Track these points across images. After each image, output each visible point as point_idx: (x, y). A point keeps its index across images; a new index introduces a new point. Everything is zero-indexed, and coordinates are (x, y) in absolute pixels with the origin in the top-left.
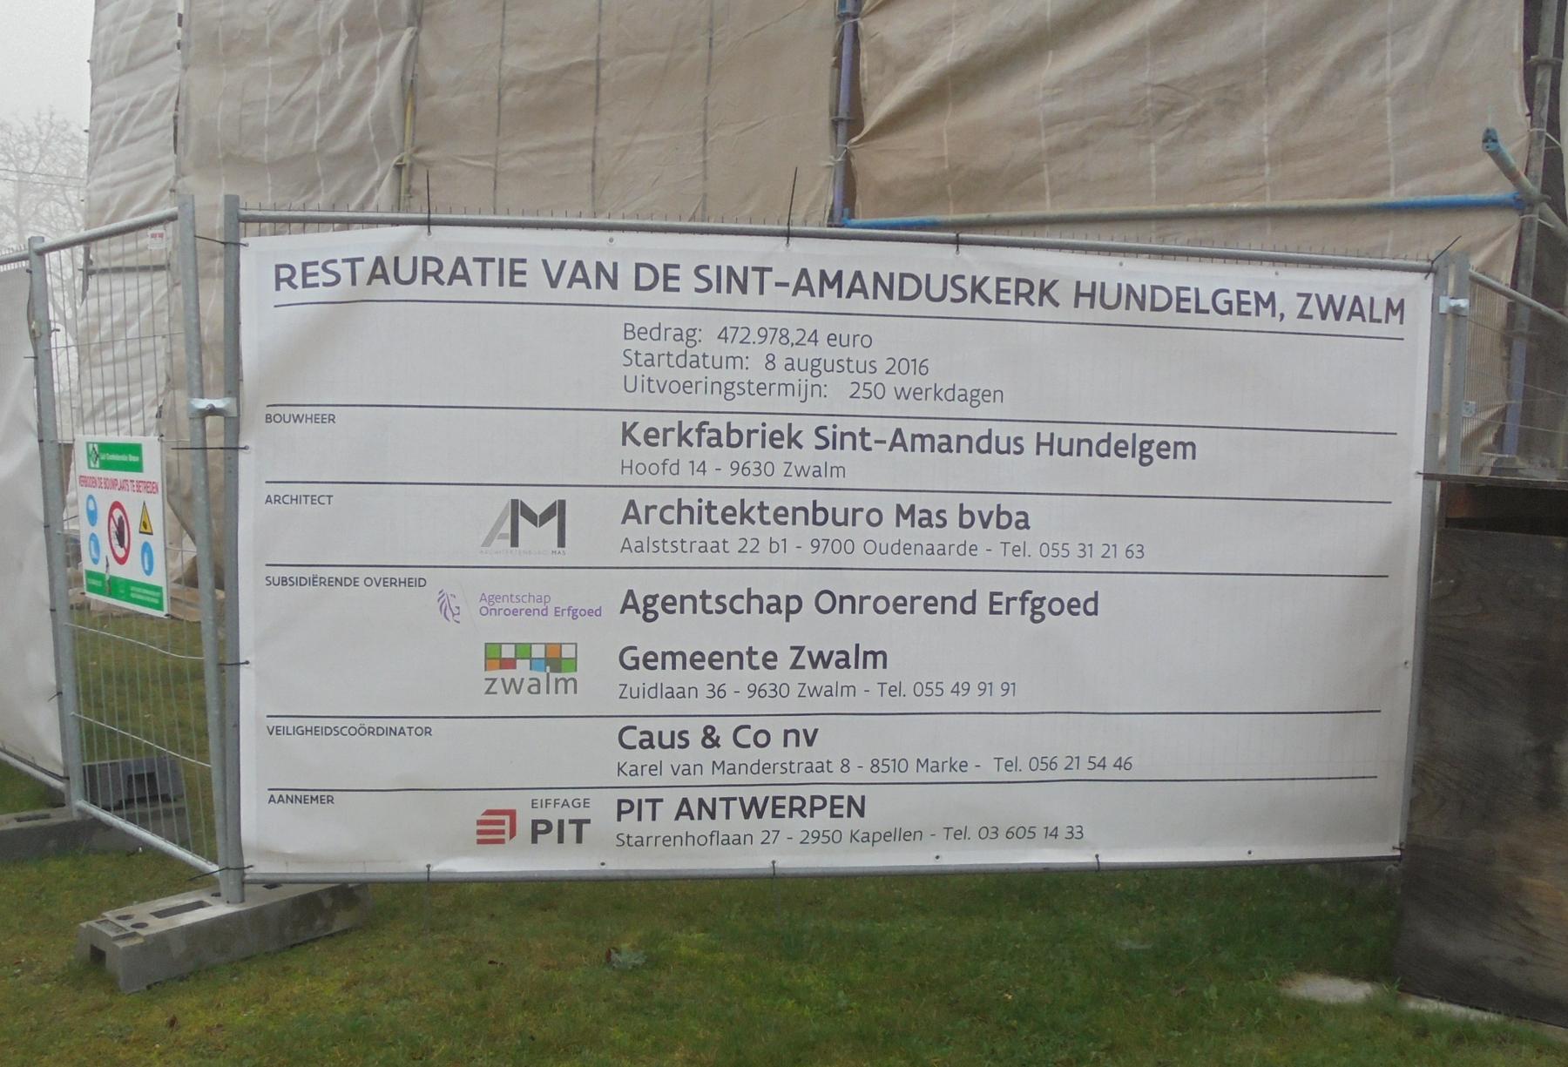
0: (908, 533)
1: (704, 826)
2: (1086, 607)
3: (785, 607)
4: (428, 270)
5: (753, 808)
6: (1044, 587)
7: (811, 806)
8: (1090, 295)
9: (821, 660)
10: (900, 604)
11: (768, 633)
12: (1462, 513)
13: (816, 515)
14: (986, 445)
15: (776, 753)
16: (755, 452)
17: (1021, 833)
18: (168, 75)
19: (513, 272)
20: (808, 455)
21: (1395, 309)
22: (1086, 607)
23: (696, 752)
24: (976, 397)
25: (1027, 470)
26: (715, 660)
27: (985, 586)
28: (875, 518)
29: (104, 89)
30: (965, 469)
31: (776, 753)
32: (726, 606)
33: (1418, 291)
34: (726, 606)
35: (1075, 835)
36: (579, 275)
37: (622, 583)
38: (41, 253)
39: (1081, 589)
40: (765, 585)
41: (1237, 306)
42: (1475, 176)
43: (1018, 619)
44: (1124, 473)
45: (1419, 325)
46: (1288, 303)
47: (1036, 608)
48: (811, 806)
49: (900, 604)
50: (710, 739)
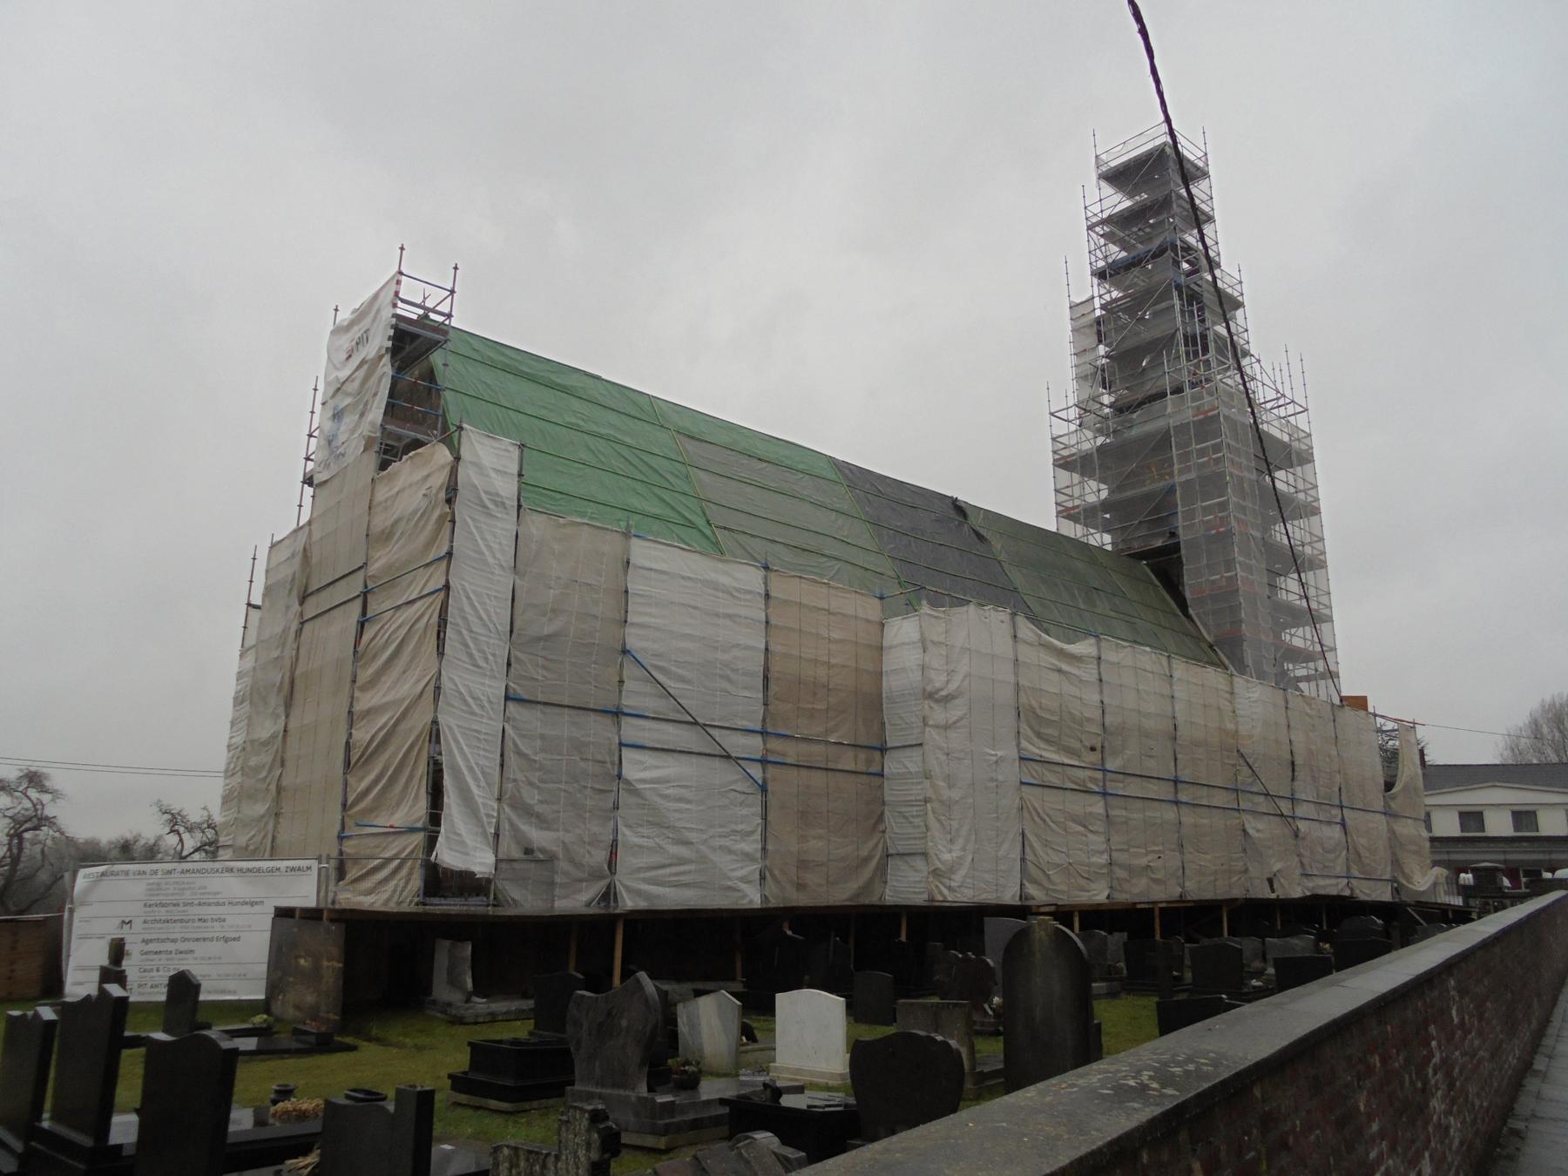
2: (238, 939)
3: (174, 941)
8: (240, 870)
12: (1116, 253)
13: (181, 921)
14: (218, 904)
15: (148, 990)
17: (223, 992)
18: (238, 778)
19: (127, 873)
20: (181, 908)
21: (309, 868)
22: (238, 939)
30: (212, 910)
31: (148, 990)
32: (163, 941)
33: (314, 864)
35: (235, 993)
37: (141, 937)
38: (767, 596)
43: (222, 943)
44: (247, 909)
47: (226, 940)
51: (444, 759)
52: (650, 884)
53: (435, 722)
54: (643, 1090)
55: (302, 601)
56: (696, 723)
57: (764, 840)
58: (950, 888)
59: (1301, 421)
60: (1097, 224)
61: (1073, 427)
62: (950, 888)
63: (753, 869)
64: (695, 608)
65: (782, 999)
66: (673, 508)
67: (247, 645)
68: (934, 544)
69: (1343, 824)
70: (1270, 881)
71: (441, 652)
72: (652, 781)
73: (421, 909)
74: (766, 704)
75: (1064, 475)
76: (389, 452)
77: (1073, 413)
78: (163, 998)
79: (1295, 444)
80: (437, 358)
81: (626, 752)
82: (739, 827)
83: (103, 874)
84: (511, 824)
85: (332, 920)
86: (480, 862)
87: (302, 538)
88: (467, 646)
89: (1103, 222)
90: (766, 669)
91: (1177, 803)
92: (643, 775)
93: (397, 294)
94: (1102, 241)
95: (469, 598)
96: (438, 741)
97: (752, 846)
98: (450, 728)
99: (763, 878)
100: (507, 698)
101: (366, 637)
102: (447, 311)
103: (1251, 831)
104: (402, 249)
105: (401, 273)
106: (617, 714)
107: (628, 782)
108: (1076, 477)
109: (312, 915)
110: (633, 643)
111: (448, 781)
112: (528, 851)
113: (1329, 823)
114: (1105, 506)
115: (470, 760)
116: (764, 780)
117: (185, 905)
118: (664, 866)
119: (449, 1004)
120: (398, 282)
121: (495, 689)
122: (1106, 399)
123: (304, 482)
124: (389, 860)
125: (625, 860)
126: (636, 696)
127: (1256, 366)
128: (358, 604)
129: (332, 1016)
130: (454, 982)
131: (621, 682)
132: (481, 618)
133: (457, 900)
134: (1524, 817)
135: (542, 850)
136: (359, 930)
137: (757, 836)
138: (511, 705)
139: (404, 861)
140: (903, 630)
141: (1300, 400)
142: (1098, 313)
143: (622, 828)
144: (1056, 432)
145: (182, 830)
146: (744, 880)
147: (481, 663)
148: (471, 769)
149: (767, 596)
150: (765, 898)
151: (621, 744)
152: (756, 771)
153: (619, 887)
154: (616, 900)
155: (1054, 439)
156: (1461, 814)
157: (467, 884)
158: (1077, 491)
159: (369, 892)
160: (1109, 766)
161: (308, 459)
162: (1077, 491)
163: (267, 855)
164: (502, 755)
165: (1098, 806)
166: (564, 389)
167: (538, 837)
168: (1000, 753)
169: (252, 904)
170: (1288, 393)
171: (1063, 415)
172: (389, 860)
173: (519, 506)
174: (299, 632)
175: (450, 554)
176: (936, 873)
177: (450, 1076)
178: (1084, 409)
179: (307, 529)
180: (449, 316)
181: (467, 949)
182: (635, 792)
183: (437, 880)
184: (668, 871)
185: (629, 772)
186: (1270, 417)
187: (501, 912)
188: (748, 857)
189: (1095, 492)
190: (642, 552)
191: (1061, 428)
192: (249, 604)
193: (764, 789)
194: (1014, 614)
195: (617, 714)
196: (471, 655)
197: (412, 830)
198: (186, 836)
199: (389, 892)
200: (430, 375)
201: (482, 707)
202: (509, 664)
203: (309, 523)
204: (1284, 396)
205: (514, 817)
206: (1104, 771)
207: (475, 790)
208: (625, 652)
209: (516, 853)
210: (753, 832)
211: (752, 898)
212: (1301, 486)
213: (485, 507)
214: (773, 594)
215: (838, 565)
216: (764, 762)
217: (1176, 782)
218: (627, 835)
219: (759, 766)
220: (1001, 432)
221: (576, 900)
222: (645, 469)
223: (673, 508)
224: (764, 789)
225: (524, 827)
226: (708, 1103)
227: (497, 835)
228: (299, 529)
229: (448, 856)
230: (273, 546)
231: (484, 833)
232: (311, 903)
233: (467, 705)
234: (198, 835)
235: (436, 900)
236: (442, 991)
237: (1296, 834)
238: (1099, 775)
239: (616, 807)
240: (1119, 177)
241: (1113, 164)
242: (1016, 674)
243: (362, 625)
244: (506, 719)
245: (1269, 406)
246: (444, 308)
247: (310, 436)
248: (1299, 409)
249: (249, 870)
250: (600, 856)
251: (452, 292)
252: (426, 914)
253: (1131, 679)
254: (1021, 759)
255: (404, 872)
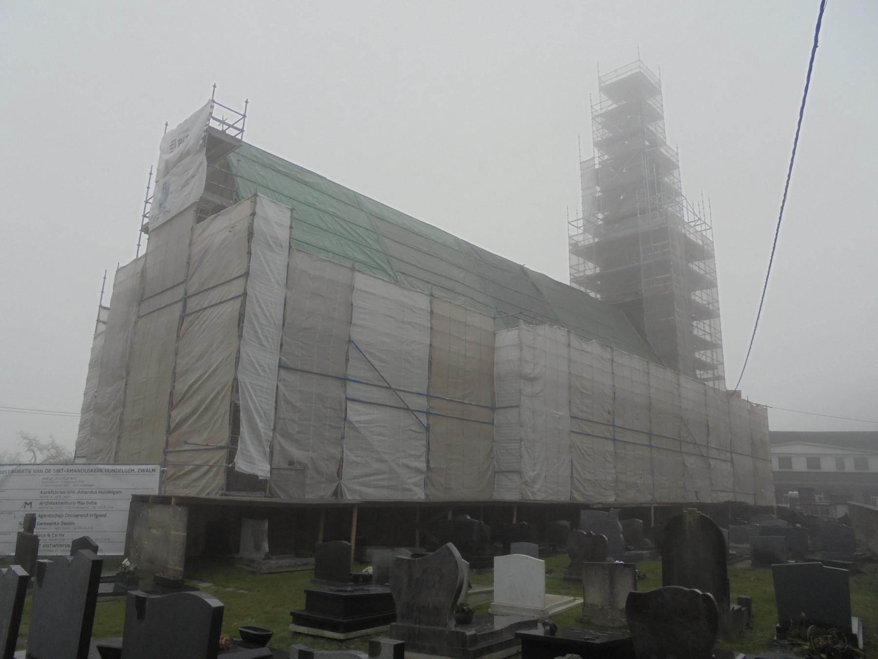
0: (79, 505)
1: (47, 548)
2: (105, 516)
3: (60, 516)
4: (19, 471)
5: (54, 546)
6: (98, 513)
7: (61, 546)
8: (107, 471)
9: (65, 524)
10: (77, 516)
11: (57, 520)
14: (92, 492)
16: (59, 495)
19: (30, 471)
20: (66, 495)
21: (154, 470)
22: (105, 516)
23: (47, 538)
24: (90, 486)
25: (94, 496)
26: (50, 524)
27: (89, 513)
28: (74, 503)
29: (274, 217)
30: (87, 496)
32: (53, 516)
33: (158, 468)
34: (53, 516)
36: (38, 471)
38: (432, 312)
39: (104, 513)
40: (58, 513)
41: (128, 471)
42: (223, 444)
44: (110, 496)
45: (158, 474)
46: (136, 470)
47: (97, 516)
48: (61, 546)
49: (77, 516)
50: (49, 535)
51: (241, 403)
52: (363, 486)
53: (236, 379)
54: (452, 626)
55: (139, 305)
56: (391, 388)
57: (428, 462)
58: (533, 493)
59: (708, 234)
60: (597, 116)
61: (580, 231)
62: (533, 493)
63: (420, 478)
64: (391, 317)
65: (498, 560)
66: (373, 259)
67: (98, 331)
68: (515, 293)
69: (732, 462)
70: (696, 492)
71: (240, 336)
72: (365, 422)
73: (224, 498)
74: (429, 378)
75: (575, 258)
76: (204, 211)
77: (581, 223)
78: (14, 554)
79: (706, 247)
80: (232, 157)
81: (350, 405)
82: (413, 453)
83: (13, 471)
84: (281, 446)
85: (178, 504)
86: (262, 469)
87: (142, 263)
88: (256, 332)
89: (600, 115)
90: (431, 357)
91: (651, 446)
92: (358, 418)
93: (211, 114)
94: (600, 127)
95: (258, 302)
96: (237, 392)
97: (422, 465)
98: (245, 383)
99: (425, 484)
100: (280, 366)
101: (185, 325)
102: (241, 127)
103: (688, 465)
104: (215, 86)
105: (214, 102)
106: (344, 380)
107: (350, 422)
108: (581, 260)
109: (163, 500)
110: (355, 337)
111: (242, 415)
112: (291, 463)
113: (725, 461)
114: (598, 277)
115: (258, 403)
116: (428, 425)
117: (69, 493)
118: (369, 475)
119: (253, 561)
120: (212, 107)
121: (273, 360)
122: (600, 216)
123: (141, 231)
124: (198, 467)
125: (347, 471)
126: (356, 369)
127: (684, 202)
128: (180, 305)
129: (178, 568)
130: (258, 548)
131: (347, 360)
132: (265, 315)
133: (244, 494)
134: (813, 461)
135: (300, 463)
136: (195, 508)
137: (423, 458)
138: (282, 372)
139: (211, 467)
140: (507, 337)
141: (708, 222)
142: (597, 166)
143: (346, 452)
144: (571, 233)
145: (35, 449)
146: (415, 484)
147: (265, 343)
148: (257, 410)
149: (432, 312)
150: (426, 495)
151: (347, 399)
152: (423, 419)
153: (345, 489)
154: (341, 495)
155: (570, 237)
156: (779, 459)
157: (252, 482)
158: (582, 268)
159: (186, 487)
160: (617, 424)
161: (144, 216)
162: (582, 268)
163: (112, 461)
164: (276, 402)
165: (610, 447)
166: (306, 183)
167: (297, 453)
168: (560, 413)
169: (114, 493)
170: (702, 218)
171: (575, 223)
172: (198, 467)
173: (290, 247)
174: (136, 323)
175: (247, 274)
176: (526, 483)
177: (292, 614)
178: (587, 220)
179: (143, 260)
180: (242, 131)
181: (266, 525)
182: (355, 429)
183: (235, 479)
184: (372, 478)
185: (352, 417)
186: (692, 230)
187: (274, 500)
188: (418, 471)
189: (591, 269)
190: (362, 281)
191: (574, 231)
192: (101, 306)
193: (427, 429)
194: (568, 332)
195: (344, 380)
196: (258, 338)
197: (221, 448)
198: (38, 453)
199: (208, 486)
200: (228, 166)
201: (264, 371)
202: (281, 345)
203: (146, 255)
204: (700, 219)
205: (282, 441)
206: (614, 426)
207: (260, 424)
208: (350, 341)
209: (284, 465)
210: (420, 456)
211: (419, 495)
212: (708, 271)
213: (270, 246)
214: (435, 311)
215: (464, 298)
216: (428, 413)
217: (650, 434)
218: (349, 456)
219: (425, 415)
220: (541, 232)
221: (317, 493)
222: (353, 233)
223: (373, 259)
224: (427, 429)
225: (289, 448)
226: (500, 633)
227: (272, 452)
228: (137, 260)
229: (242, 465)
230: (118, 270)
231: (264, 452)
232: (156, 492)
233: (256, 369)
234: (46, 452)
235: (234, 493)
236: (247, 550)
237: (709, 467)
238: (611, 428)
239: (343, 438)
240: (610, 90)
241: (607, 83)
242: (569, 367)
243: (182, 319)
244: (279, 380)
245: (692, 224)
246: (239, 125)
247: (147, 202)
248: (708, 227)
249: (113, 471)
250: (333, 468)
251: (244, 116)
252: (228, 501)
253: (631, 374)
254: (571, 417)
255: (211, 474)
